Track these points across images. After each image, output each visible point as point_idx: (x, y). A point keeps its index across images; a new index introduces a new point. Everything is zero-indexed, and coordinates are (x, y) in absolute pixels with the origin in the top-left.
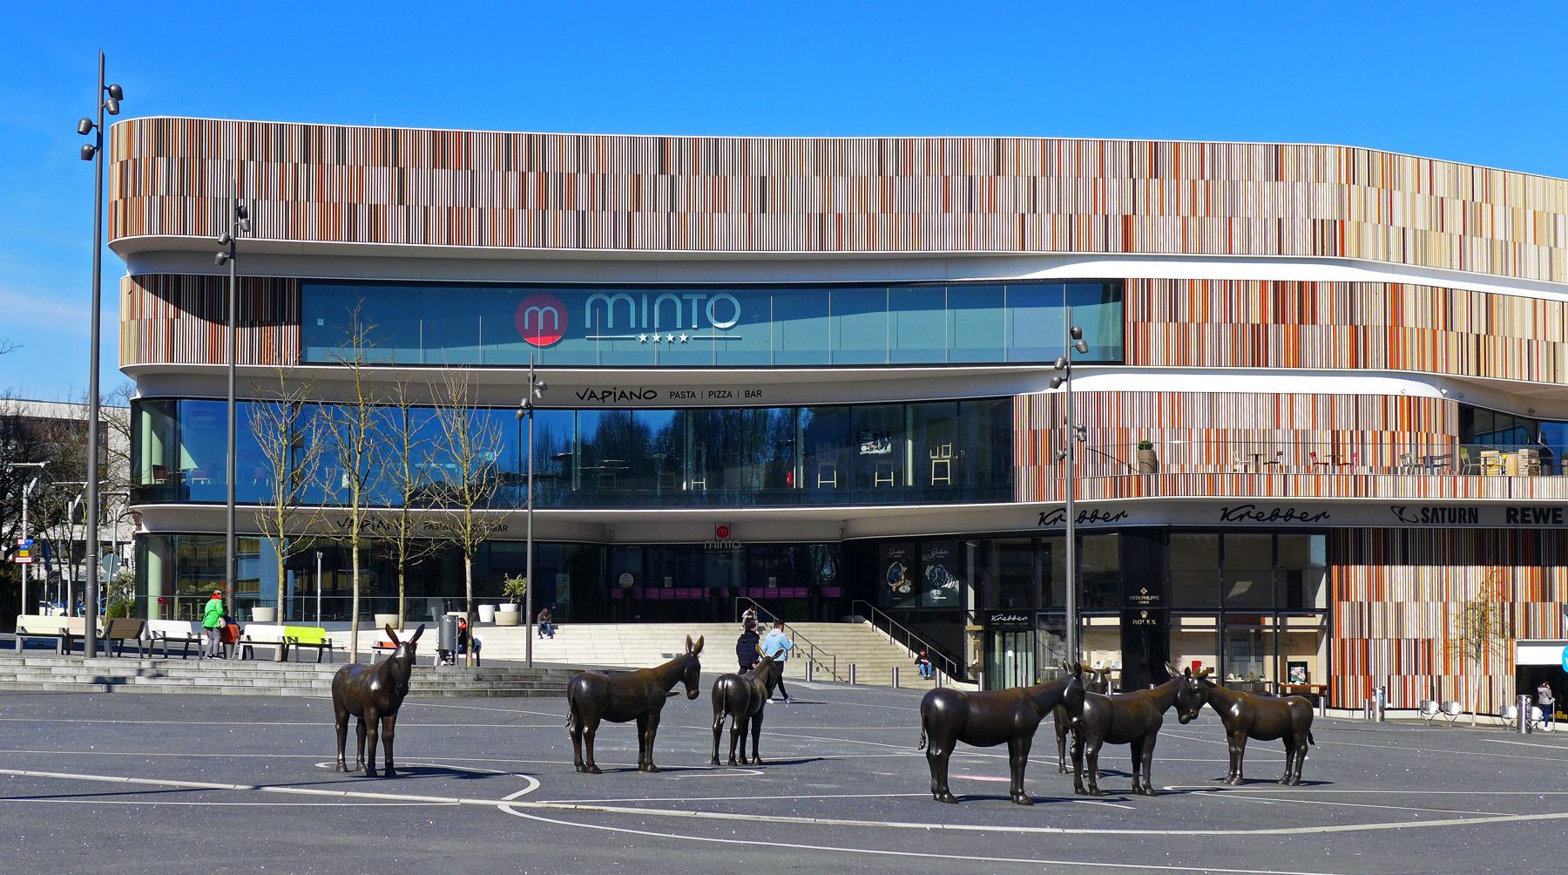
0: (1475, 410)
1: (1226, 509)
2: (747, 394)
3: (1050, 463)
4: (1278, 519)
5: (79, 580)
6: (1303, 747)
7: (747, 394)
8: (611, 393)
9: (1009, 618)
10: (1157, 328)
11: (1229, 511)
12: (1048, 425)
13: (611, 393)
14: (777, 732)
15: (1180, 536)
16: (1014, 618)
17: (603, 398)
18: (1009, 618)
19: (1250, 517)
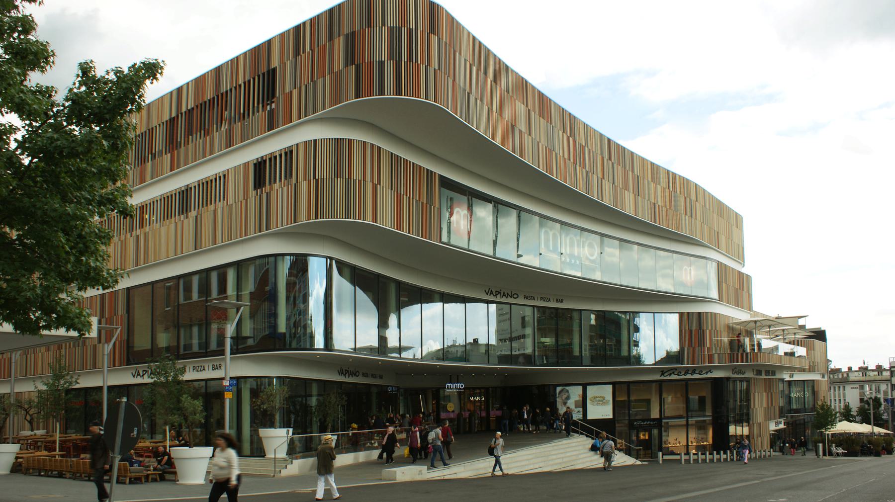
0: (497, 363)
1: (663, 371)
2: (502, 331)
3: (699, 346)
4: (695, 374)
5: (514, 353)
6: (29, 237)
7: (502, 331)
8: (499, 293)
9: (645, 423)
10: (724, 284)
11: (664, 372)
12: (697, 328)
13: (499, 293)
14: (173, 144)
15: (692, 382)
16: (648, 423)
17: (496, 295)
18: (645, 423)
19: (675, 374)
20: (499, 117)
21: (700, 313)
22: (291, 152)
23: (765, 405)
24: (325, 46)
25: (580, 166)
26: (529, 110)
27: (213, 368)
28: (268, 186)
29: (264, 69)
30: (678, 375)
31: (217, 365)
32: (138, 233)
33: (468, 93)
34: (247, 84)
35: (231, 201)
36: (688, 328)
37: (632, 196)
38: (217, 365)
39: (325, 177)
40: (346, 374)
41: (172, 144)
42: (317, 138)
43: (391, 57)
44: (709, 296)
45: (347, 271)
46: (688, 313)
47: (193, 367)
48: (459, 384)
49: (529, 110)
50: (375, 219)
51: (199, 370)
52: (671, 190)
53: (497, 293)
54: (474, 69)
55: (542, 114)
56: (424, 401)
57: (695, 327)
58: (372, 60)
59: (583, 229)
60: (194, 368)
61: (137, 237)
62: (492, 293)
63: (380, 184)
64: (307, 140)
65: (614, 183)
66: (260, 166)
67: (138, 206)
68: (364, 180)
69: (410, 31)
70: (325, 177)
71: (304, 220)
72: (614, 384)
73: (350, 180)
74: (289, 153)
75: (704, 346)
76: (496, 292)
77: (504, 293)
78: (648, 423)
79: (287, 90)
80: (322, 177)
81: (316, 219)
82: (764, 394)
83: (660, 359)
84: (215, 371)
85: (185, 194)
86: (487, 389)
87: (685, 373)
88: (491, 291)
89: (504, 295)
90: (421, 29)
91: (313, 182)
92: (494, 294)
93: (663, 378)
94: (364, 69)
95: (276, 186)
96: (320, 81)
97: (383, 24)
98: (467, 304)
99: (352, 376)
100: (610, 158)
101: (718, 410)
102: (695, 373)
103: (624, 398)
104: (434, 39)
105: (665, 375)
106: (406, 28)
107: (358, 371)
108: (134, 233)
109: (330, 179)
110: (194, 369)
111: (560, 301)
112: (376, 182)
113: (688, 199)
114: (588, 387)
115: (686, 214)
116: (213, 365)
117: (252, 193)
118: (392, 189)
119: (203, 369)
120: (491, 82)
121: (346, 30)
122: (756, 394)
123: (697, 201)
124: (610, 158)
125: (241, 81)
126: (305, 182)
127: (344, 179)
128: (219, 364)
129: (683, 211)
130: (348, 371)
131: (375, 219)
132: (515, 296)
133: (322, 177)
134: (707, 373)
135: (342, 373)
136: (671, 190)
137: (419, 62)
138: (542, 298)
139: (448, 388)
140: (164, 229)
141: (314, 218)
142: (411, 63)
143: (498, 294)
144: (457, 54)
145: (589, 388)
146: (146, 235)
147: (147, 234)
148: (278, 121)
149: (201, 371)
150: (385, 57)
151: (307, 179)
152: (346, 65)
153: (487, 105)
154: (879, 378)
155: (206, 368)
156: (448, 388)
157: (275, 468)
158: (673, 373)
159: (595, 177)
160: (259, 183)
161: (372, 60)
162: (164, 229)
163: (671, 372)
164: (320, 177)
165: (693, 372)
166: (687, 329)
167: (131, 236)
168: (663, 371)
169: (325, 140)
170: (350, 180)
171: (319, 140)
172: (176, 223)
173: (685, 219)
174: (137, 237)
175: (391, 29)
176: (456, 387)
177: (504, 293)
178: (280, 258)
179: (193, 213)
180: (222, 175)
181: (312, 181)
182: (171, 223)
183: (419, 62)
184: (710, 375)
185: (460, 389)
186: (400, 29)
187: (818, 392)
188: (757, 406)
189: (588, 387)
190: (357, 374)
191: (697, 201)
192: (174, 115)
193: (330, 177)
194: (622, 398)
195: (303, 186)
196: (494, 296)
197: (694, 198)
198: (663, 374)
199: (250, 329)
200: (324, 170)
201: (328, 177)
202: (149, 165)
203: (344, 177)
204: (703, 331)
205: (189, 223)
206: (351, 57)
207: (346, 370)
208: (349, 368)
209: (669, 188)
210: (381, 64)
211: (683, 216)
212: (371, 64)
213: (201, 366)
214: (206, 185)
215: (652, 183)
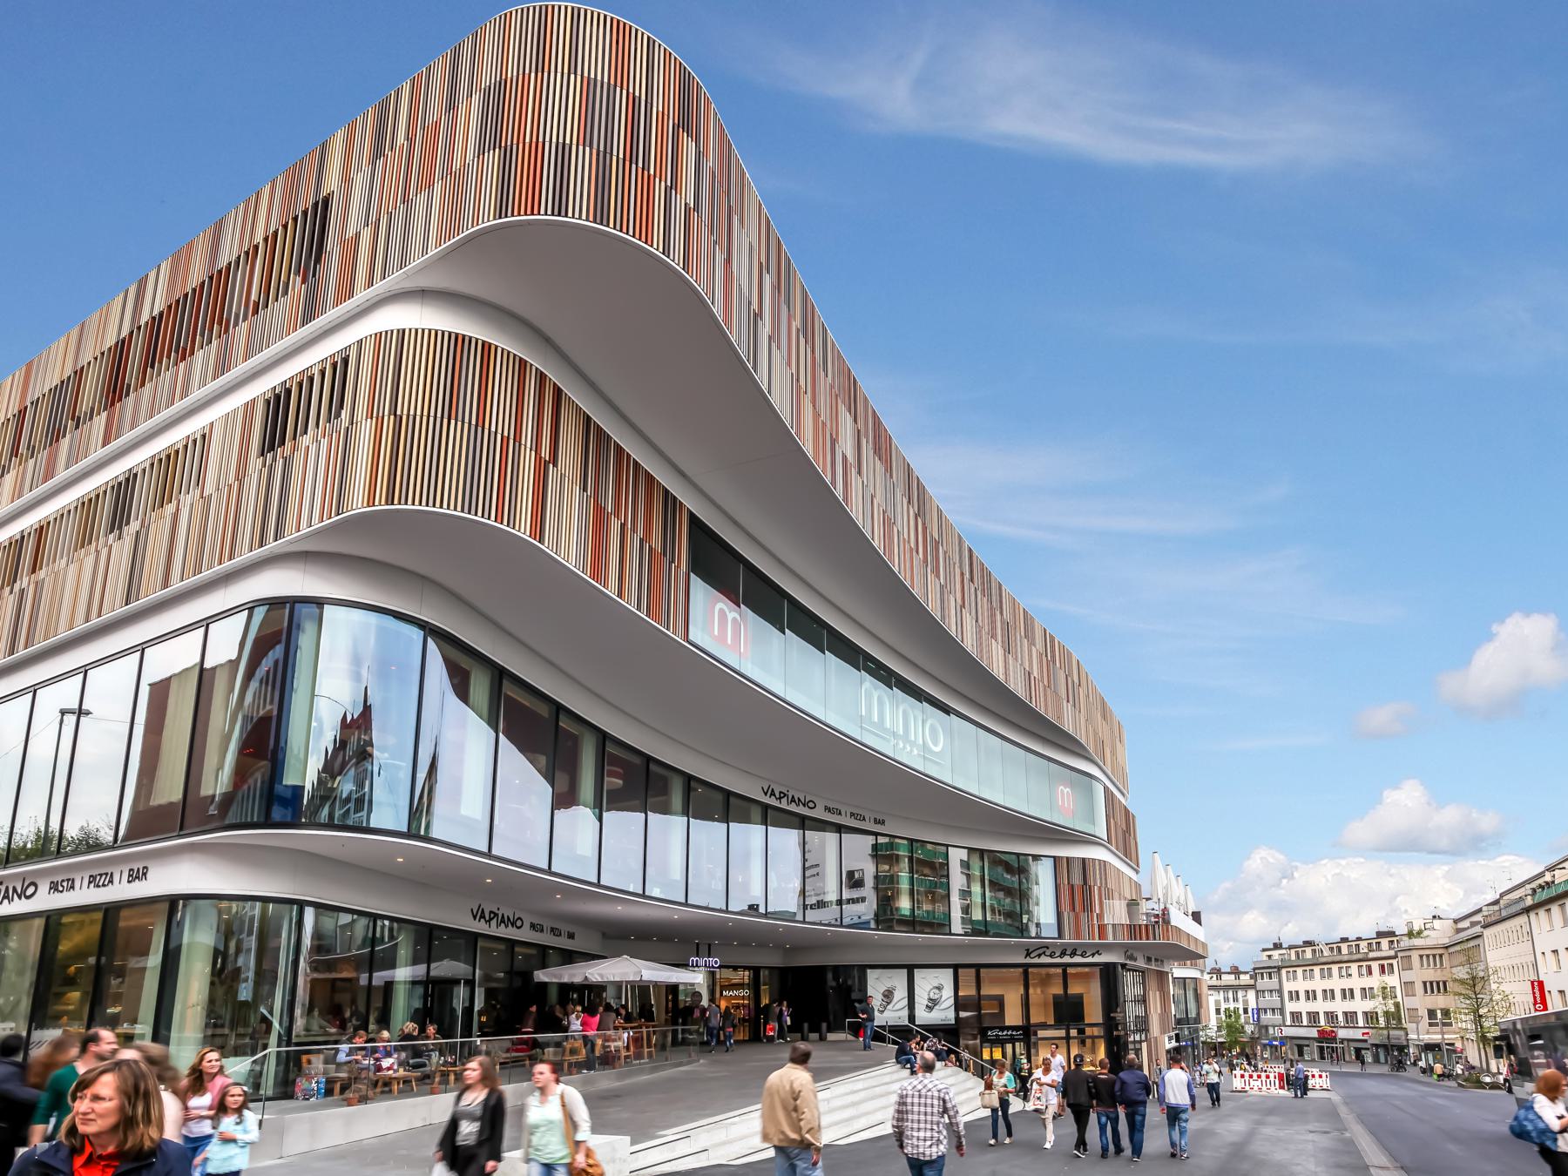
3: (1084, 911)
8: (785, 795)
12: (1082, 883)
14: (114, 392)
16: (1010, 1033)
17: (780, 798)
20: (810, 406)
21: (1084, 859)
22: (346, 361)
23: (1159, 1012)
24: (437, 124)
25: (932, 572)
26: (859, 431)
27: (129, 876)
28: (288, 444)
29: (306, 200)
30: (1051, 956)
31: (138, 869)
32: (25, 585)
33: (755, 314)
34: (272, 239)
35: (209, 488)
36: (1069, 883)
37: (1001, 651)
38: (138, 869)
39: (419, 412)
40: (491, 919)
41: (115, 391)
42: (406, 326)
43: (587, 140)
44: (1097, 835)
45: (480, 686)
46: (1067, 858)
47: (91, 876)
48: (711, 959)
49: (859, 431)
50: (538, 530)
51: (101, 884)
52: (1049, 658)
53: (782, 795)
54: (767, 279)
55: (877, 451)
56: (436, 630)
57: (1077, 880)
58: (541, 139)
59: (821, 924)
60: (92, 879)
61: (22, 591)
62: (773, 794)
63: (555, 465)
64: (383, 329)
65: (977, 621)
66: (278, 404)
67: (34, 528)
68: (518, 438)
69: (634, 101)
70: (419, 412)
71: (359, 506)
72: (956, 968)
73: (480, 429)
74: (340, 365)
75: (1091, 911)
76: (781, 792)
77: (793, 797)
78: (1010, 1033)
79: (351, 233)
80: (412, 412)
81: (387, 504)
82: (1158, 993)
83: (1508, 621)
84: (133, 884)
85: (124, 489)
86: (756, 971)
87: (1061, 954)
88: (773, 790)
89: (793, 800)
90: (661, 109)
91: (388, 423)
92: (778, 796)
93: (1028, 960)
94: (521, 160)
95: (306, 440)
96: (421, 200)
97: (573, 69)
98: (731, 824)
99: (507, 926)
100: (972, 580)
101: (1112, 1015)
102: (1075, 954)
103: (972, 992)
104: (689, 148)
105: (1032, 955)
106: (624, 92)
107: (519, 918)
108: (17, 587)
109: (432, 419)
110: (90, 882)
111: (879, 823)
112: (545, 453)
113: (1069, 679)
114: (915, 970)
115: (1068, 701)
116: (130, 870)
117: (255, 463)
118: (585, 489)
119: (109, 882)
120: (798, 330)
121: (487, 78)
122: (1151, 992)
123: (1080, 685)
124: (972, 580)
125: (259, 238)
126: (369, 420)
127: (466, 425)
128: (144, 868)
129: (1064, 696)
130: (496, 915)
131: (538, 530)
132: (811, 805)
133: (412, 412)
134: (1093, 955)
135: (482, 916)
136: (1049, 658)
137: (652, 172)
138: (852, 814)
139: (693, 965)
140: (73, 568)
141: (383, 502)
142: (634, 166)
143: (783, 797)
144: (735, 219)
145: (918, 973)
146: (39, 586)
147: (39, 585)
148: (325, 302)
149: (104, 885)
150: (572, 136)
151: (375, 415)
152: (481, 152)
153: (789, 364)
154: (1237, 983)
155: (116, 878)
156: (693, 965)
157: (263, 1115)
158: (1044, 953)
159: (952, 599)
160: (273, 439)
161: (541, 139)
162: (73, 568)
163: (1040, 951)
164: (405, 412)
165: (1073, 954)
166: (1066, 883)
167: (11, 592)
168: (1028, 950)
169: (426, 332)
170: (480, 429)
171: (410, 330)
172: (97, 551)
173: (1067, 708)
174: (22, 591)
175: (590, 85)
176: (706, 965)
177: (793, 797)
178: (304, 610)
179: (134, 526)
180: (198, 436)
181: (386, 418)
182: (87, 554)
183: (652, 172)
184: (1097, 959)
185: (713, 967)
186: (611, 90)
187: (1200, 994)
188: (1152, 1012)
189: (915, 970)
190: (519, 923)
191: (1080, 685)
192: (125, 333)
193: (432, 414)
194: (967, 991)
195: (366, 429)
196: (777, 799)
197: (1076, 681)
198: (1028, 954)
199: (654, 1070)
200: (416, 397)
201: (425, 413)
202: (65, 443)
203: (467, 420)
204: (1090, 886)
205: (121, 549)
206: (492, 135)
207: (491, 912)
208: (498, 909)
209: (1046, 656)
210: (563, 150)
211: (1065, 702)
212: (537, 148)
213: (107, 874)
214: (168, 461)
215: (1026, 640)
